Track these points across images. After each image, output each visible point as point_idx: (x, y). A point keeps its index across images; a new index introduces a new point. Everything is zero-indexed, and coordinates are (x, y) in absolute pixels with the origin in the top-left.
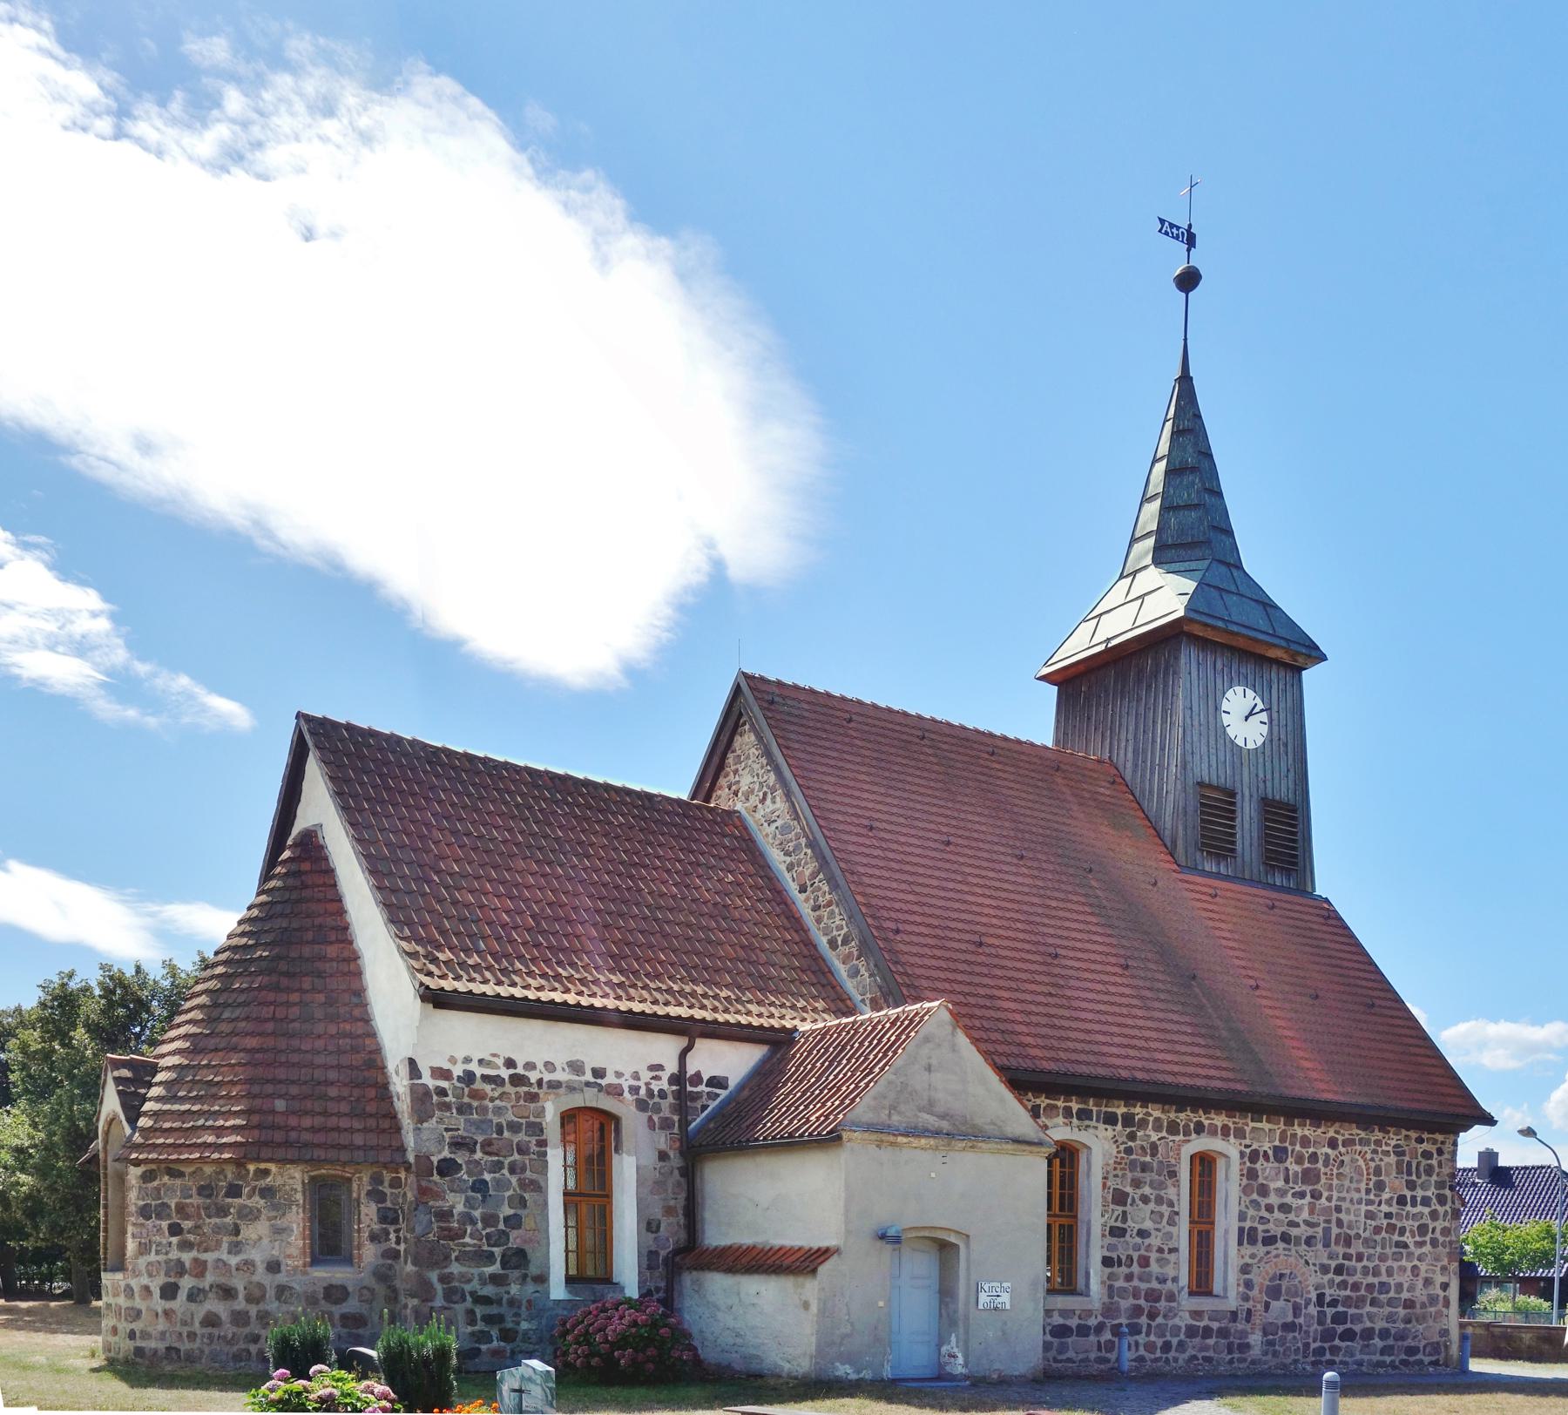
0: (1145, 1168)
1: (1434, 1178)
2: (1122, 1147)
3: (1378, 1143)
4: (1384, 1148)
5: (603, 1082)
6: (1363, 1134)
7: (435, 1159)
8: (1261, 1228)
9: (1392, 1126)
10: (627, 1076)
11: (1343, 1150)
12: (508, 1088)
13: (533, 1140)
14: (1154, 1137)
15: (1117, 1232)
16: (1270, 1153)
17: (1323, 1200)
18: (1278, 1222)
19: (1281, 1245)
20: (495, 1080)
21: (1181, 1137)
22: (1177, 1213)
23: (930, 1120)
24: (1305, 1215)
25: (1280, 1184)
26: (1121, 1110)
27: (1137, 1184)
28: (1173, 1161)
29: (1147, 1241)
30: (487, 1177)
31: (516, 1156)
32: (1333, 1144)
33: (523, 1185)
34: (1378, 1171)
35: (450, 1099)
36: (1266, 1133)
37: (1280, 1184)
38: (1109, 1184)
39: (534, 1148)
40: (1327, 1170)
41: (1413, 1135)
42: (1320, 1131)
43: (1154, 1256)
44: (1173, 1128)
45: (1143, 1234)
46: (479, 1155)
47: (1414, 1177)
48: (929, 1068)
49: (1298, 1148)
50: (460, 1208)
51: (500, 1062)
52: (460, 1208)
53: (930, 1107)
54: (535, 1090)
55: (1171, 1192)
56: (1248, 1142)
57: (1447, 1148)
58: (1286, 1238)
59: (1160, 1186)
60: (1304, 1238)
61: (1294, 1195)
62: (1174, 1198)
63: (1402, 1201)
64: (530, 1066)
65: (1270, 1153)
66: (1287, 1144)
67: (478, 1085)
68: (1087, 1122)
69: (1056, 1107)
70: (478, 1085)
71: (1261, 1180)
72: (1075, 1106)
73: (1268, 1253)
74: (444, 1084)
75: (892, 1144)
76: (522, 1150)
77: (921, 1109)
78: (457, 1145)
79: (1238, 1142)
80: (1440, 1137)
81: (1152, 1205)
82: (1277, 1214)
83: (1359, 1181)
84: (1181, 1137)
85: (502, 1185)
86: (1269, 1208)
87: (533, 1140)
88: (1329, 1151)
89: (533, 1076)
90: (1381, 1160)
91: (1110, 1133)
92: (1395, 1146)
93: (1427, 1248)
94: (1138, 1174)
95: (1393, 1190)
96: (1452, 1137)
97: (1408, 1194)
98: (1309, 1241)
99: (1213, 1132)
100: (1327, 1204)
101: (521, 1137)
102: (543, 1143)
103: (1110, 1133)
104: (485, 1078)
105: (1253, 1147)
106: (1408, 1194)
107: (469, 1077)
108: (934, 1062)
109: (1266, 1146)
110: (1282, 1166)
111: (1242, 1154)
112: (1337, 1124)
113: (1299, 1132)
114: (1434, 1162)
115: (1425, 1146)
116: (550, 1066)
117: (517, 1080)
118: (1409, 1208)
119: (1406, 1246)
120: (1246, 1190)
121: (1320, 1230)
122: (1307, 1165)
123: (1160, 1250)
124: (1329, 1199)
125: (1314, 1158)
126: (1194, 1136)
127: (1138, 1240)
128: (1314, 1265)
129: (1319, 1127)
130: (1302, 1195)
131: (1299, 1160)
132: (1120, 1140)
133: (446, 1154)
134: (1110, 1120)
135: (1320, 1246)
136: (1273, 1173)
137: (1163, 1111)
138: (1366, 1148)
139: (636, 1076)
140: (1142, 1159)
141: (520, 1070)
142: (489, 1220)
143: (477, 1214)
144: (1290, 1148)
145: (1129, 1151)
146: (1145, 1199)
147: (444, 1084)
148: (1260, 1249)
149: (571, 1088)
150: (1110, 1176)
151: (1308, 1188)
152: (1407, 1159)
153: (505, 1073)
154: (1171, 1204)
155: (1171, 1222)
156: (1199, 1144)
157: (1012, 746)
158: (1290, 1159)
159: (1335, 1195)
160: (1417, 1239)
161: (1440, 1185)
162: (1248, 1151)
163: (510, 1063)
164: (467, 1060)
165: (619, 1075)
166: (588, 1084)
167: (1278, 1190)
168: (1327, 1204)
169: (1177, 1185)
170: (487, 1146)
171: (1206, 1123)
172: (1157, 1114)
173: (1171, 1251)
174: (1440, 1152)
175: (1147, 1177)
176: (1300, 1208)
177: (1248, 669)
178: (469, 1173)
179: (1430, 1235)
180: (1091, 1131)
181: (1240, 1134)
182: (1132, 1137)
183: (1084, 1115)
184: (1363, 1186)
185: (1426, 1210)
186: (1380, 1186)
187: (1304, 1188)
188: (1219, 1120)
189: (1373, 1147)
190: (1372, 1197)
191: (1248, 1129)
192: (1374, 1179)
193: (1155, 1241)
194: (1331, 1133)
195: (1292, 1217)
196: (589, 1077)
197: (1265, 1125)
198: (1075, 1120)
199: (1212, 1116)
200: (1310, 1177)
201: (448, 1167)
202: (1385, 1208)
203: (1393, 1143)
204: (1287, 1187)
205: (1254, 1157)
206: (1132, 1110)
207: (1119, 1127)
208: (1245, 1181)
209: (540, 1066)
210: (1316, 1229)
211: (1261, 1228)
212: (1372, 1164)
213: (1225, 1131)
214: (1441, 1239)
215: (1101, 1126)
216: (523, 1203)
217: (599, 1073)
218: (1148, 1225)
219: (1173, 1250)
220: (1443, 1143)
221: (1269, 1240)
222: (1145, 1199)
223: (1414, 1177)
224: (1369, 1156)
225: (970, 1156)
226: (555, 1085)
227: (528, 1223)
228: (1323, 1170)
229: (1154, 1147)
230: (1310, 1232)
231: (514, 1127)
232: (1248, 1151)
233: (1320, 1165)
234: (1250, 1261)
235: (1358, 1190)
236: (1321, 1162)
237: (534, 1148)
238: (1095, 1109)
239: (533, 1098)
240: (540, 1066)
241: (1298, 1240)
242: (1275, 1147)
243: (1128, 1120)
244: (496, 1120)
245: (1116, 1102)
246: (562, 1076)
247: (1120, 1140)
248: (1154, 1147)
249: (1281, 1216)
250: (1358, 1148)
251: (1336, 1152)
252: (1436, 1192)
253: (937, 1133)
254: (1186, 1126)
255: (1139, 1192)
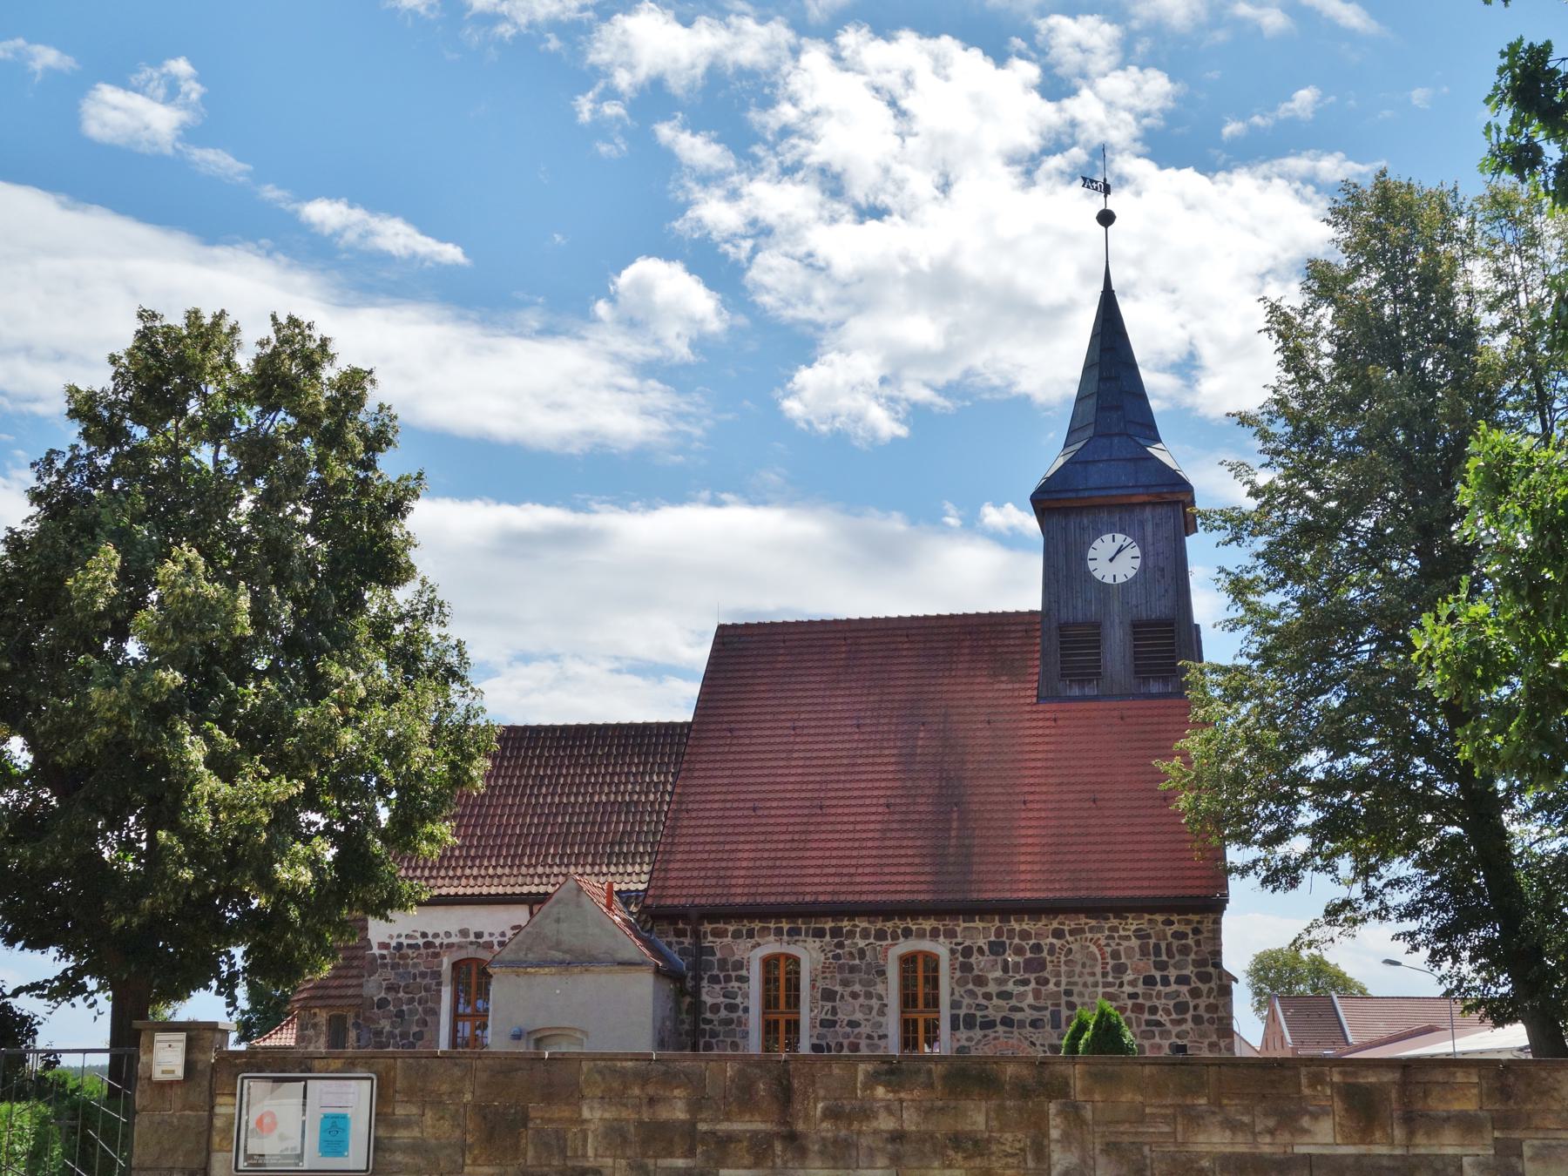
0: (853, 969)
1: (1193, 956)
2: (830, 955)
3: (1114, 929)
4: (1122, 933)
5: (481, 941)
6: (1093, 923)
7: (376, 999)
8: (979, 1014)
9: (1130, 912)
10: (497, 935)
11: (1070, 939)
12: (423, 951)
13: (434, 982)
14: (861, 943)
15: (828, 1024)
16: (986, 948)
17: (1051, 986)
18: (997, 1008)
19: (1000, 1028)
20: (416, 947)
21: (889, 941)
22: (886, 1005)
23: (558, 955)
24: (1030, 1000)
25: (999, 974)
26: (829, 925)
27: (845, 983)
28: (882, 962)
29: (857, 1030)
30: (405, 1007)
31: (423, 993)
32: (1058, 934)
33: (426, 1012)
34: (1116, 955)
35: (388, 960)
36: (981, 933)
37: (999, 974)
38: (818, 984)
39: (434, 987)
40: (1054, 958)
41: (1159, 918)
42: (1040, 924)
43: (863, 1043)
44: (881, 935)
45: (853, 1024)
46: (401, 994)
47: (1164, 958)
48: (558, 921)
49: (1016, 941)
50: (388, 1028)
51: (418, 935)
52: (388, 1028)
53: (557, 946)
54: (438, 950)
55: (880, 988)
56: (959, 940)
57: (1207, 925)
58: (1006, 1022)
59: (871, 983)
60: (1028, 1021)
61: (1015, 983)
62: (883, 993)
63: (1150, 981)
64: (436, 935)
65: (986, 948)
66: (1004, 939)
67: (405, 951)
68: (796, 938)
69: (769, 928)
70: (405, 951)
71: (976, 972)
72: (785, 926)
73: (985, 1036)
74: (385, 952)
75: (526, 973)
76: (427, 990)
77: (550, 948)
78: (389, 989)
79: (947, 941)
80: (1196, 918)
81: (861, 1000)
82: (995, 1001)
83: (1092, 966)
84: (889, 941)
85: (412, 1012)
86: (988, 996)
87: (434, 982)
88: (1054, 941)
89: (437, 942)
90: (1118, 944)
91: (818, 944)
92: (1135, 931)
93: (1188, 1026)
94: (847, 975)
95: (1136, 970)
96: (1212, 916)
97: (1158, 975)
98: (1035, 1024)
99: (921, 934)
100: (1055, 989)
101: (427, 981)
102: (439, 984)
103: (818, 944)
104: (409, 946)
105: (966, 944)
106: (1158, 975)
107: (400, 945)
108: (562, 916)
109: (981, 942)
110: (999, 959)
111: (953, 952)
112: (1061, 917)
113: (1017, 927)
114: (1190, 941)
115: (1175, 927)
116: (448, 934)
117: (428, 945)
118: (1159, 987)
119: (1159, 1024)
120: (962, 982)
121: (1047, 1013)
122: (1028, 955)
123: (869, 1037)
124: (1057, 984)
125: (1037, 948)
126: (902, 939)
127: (848, 1029)
128: (1043, 1045)
129: (1040, 920)
130: (1025, 982)
131: (1019, 951)
132: (828, 949)
133: (383, 995)
134: (819, 933)
135: (1048, 1028)
136: (988, 965)
137: (869, 922)
138: (1099, 935)
139: (503, 934)
140: (851, 963)
141: (430, 939)
142: (404, 1035)
143: (397, 1031)
144: (1008, 942)
145: (837, 957)
146: (855, 995)
147: (385, 952)
148: (978, 1033)
149: (460, 946)
150: (819, 978)
151: (1032, 977)
152: (1152, 941)
153: (421, 941)
154: (880, 998)
155: (882, 1013)
156: (905, 946)
157: (933, 623)
158: (1008, 952)
159: (1064, 980)
160: (1174, 1016)
161: (1196, 963)
162: (960, 948)
163: (424, 935)
164: (399, 936)
165: (491, 935)
166: (471, 943)
167: (996, 980)
168: (1055, 989)
169: (885, 982)
170: (407, 989)
171: (914, 928)
172: (865, 925)
173: (880, 1037)
174: (1196, 931)
175: (856, 977)
176: (1022, 995)
177: (1104, 516)
178: (394, 1006)
179: (1191, 1012)
180: (800, 944)
181: (951, 934)
182: (840, 945)
183: (794, 932)
184: (1098, 970)
185: (1184, 989)
186: (1120, 969)
187: (1026, 976)
188: (927, 925)
189: (1107, 933)
190: (1110, 979)
191: (959, 930)
192: (1111, 962)
193: (865, 1029)
194: (1055, 925)
195: (1013, 1002)
196: (472, 938)
197: (979, 924)
198: (785, 938)
199: (920, 921)
200: (1036, 965)
201: (383, 1003)
202: (1128, 989)
203: (1134, 927)
204: (1006, 976)
205: (967, 952)
206: (840, 924)
207: (828, 938)
208: (958, 974)
209: (442, 934)
210: (1044, 1013)
211: (979, 1014)
212: (1108, 949)
213: (935, 934)
214: (1206, 1016)
215: (810, 939)
216: (425, 1023)
217: (479, 935)
218: (858, 1016)
219: (885, 1036)
220: (1198, 922)
221: (988, 1025)
222: (855, 995)
223: (1164, 958)
224: (1103, 942)
225: (587, 977)
226: (450, 946)
227: (427, 1036)
228: (1049, 958)
229: (862, 953)
230: (1036, 1015)
231: (423, 975)
232: (960, 948)
233: (1045, 954)
234: (966, 1044)
235: (1093, 974)
236: (1045, 952)
237: (434, 987)
238: (803, 927)
239: (436, 955)
240: (442, 934)
241: (1021, 1024)
242: (990, 943)
243: (836, 932)
244: (413, 971)
245: (823, 920)
246: (454, 940)
247: (828, 949)
248: (862, 953)
249: (1001, 1002)
250: (1089, 936)
251: (1063, 942)
252: (1195, 970)
253: (561, 963)
254: (894, 932)
255: (849, 989)
